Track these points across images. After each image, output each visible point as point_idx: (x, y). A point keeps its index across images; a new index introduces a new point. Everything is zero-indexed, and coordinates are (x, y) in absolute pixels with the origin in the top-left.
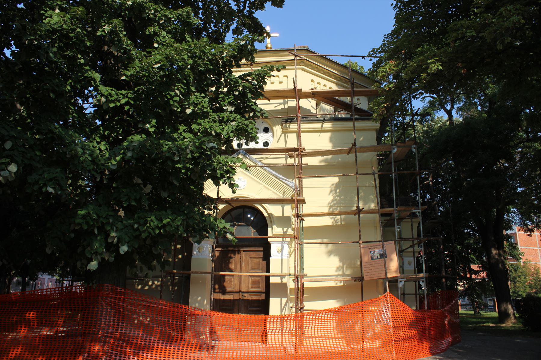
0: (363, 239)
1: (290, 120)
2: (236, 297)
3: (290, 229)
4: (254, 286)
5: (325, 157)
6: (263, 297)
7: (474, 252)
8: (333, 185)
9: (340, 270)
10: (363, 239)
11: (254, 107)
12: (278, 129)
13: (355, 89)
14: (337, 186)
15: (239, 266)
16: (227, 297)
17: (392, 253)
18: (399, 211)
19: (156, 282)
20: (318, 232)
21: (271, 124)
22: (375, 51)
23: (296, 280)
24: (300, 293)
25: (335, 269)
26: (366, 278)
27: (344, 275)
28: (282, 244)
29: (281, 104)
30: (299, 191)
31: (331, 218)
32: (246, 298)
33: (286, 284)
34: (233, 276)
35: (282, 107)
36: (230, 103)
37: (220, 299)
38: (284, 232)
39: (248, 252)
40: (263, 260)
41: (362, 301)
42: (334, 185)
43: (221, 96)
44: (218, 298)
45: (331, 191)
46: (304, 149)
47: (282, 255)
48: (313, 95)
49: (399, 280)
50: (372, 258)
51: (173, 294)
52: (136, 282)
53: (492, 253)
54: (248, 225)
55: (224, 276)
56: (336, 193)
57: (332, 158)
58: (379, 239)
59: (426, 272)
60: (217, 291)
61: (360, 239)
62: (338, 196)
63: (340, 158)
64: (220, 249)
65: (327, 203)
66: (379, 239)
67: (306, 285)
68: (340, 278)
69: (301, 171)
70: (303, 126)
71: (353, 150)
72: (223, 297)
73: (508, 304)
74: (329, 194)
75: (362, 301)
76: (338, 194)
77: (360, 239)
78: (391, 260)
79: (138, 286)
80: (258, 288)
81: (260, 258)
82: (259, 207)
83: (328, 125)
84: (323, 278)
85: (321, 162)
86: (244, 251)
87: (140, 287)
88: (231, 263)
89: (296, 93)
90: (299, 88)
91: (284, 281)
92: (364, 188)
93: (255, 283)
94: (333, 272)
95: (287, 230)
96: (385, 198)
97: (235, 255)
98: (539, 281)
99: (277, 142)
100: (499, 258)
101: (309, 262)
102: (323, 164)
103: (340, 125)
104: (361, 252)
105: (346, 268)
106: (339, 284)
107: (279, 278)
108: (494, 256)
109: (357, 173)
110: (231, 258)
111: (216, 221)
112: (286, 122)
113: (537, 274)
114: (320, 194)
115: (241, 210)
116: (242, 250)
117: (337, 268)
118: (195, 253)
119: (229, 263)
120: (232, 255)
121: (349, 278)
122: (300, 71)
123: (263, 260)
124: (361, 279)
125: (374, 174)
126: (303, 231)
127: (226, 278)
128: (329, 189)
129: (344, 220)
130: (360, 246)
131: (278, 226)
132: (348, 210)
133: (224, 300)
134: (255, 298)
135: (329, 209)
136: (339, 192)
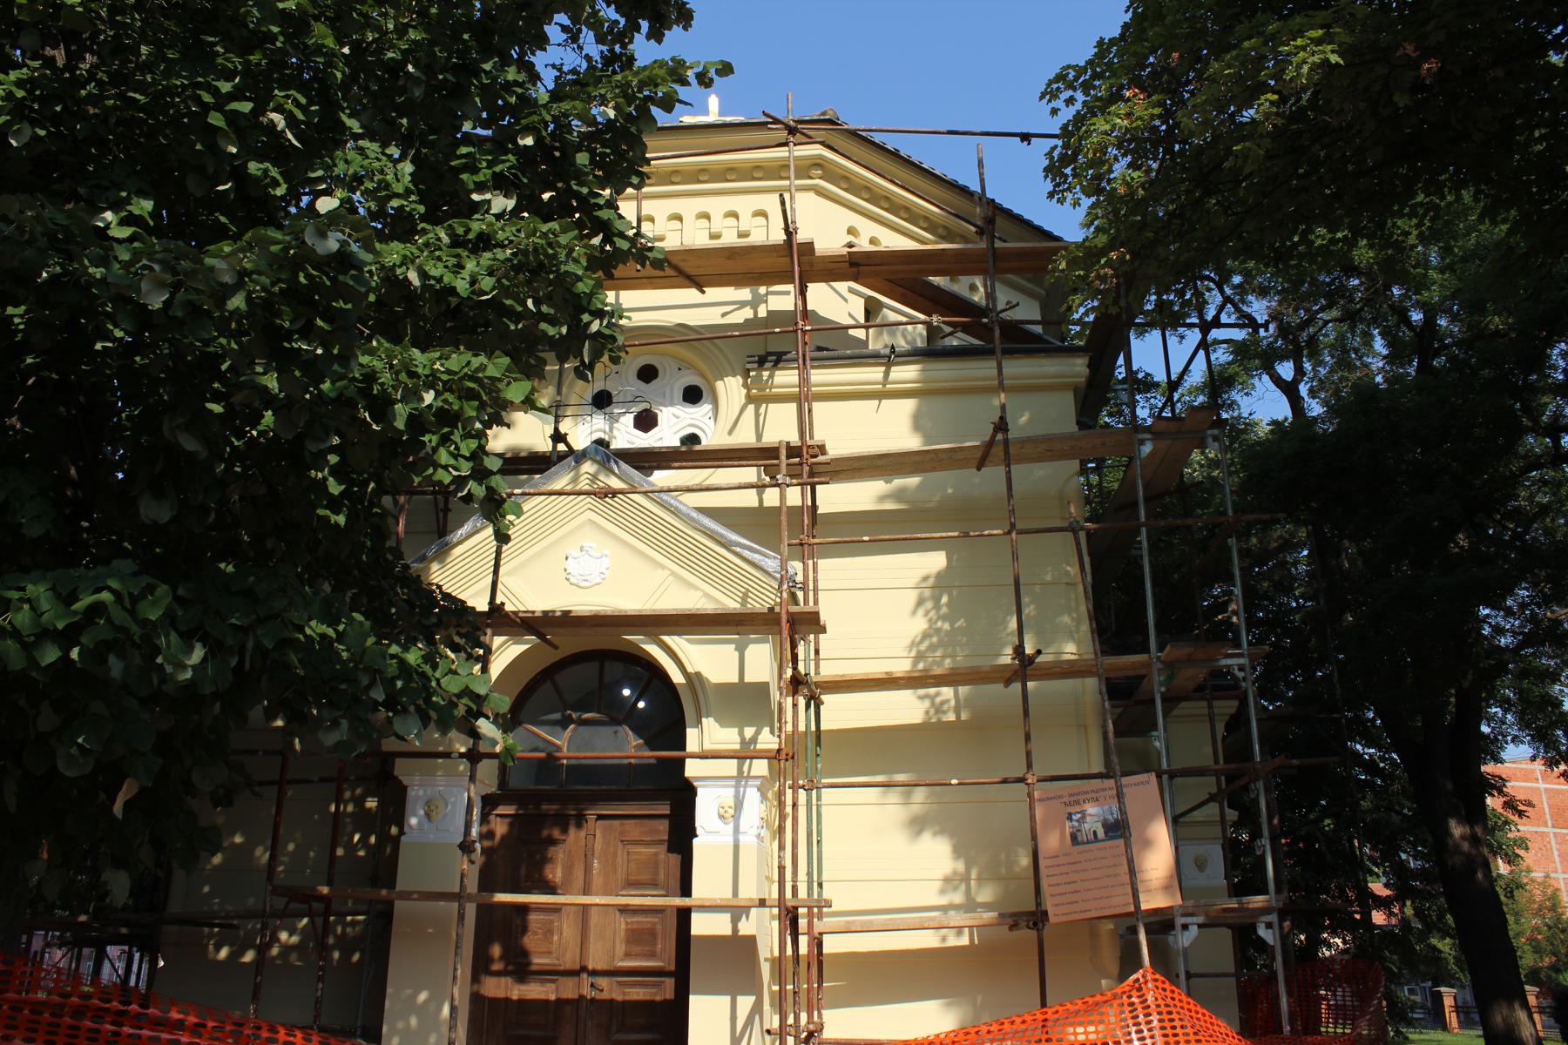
0: (1040, 769)
1: (778, 359)
2: (568, 989)
3: (766, 730)
4: (636, 949)
5: (898, 482)
6: (667, 989)
7: (1370, 836)
8: (925, 578)
9: (955, 889)
10: (1040, 769)
11: (605, 214)
12: (731, 389)
13: (998, 244)
14: (941, 583)
15: (579, 873)
16: (534, 991)
17: (1150, 818)
18: (1171, 667)
19: (284, 936)
20: (874, 752)
21: (710, 377)
22: (1072, 74)
23: (790, 918)
24: (810, 975)
25: (938, 884)
26: (1056, 912)
27: (970, 906)
28: (737, 787)
29: (743, 304)
30: (804, 588)
31: (921, 698)
32: (605, 996)
33: (751, 941)
34: (556, 909)
35: (747, 313)
36: (501, 184)
37: (507, 1000)
38: (743, 741)
39: (616, 823)
40: (670, 850)
41: (1044, 1004)
42: (931, 582)
43: (464, 150)
44: (501, 994)
45: (920, 602)
46: (822, 449)
47: (736, 831)
48: (854, 266)
49: (1180, 921)
50: (1074, 838)
51: (320, 979)
52: (211, 936)
53: (1450, 835)
54: (615, 721)
55: (524, 909)
56: (937, 607)
57: (920, 487)
58: (1097, 767)
59: (1278, 891)
60: (497, 966)
61: (1029, 766)
62: (944, 618)
63: (949, 483)
64: (510, 810)
65: (909, 641)
66: (1097, 767)
67: (831, 945)
68: (957, 918)
69: (811, 534)
70: (821, 377)
71: (998, 451)
72: (517, 991)
73: (1517, 1006)
74: (914, 612)
75: (1044, 1004)
76: (944, 610)
77: (1029, 766)
78: (1147, 843)
79: (218, 949)
80: (652, 955)
81: (660, 842)
82: (654, 650)
83: (906, 373)
84: (894, 918)
85: (882, 498)
86: (600, 817)
87: (224, 953)
88: (551, 860)
89: (795, 262)
90: (801, 237)
91: (745, 928)
92: (1037, 588)
93: (639, 939)
94: (931, 895)
95: (758, 733)
96: (1115, 624)
97: (565, 831)
98: (1563, 931)
99: (730, 433)
100: (1474, 852)
101: (838, 859)
102: (890, 506)
103: (947, 371)
104: (1032, 817)
105: (979, 879)
106: (953, 941)
107: (727, 917)
108: (1457, 846)
109: (1013, 526)
110: (553, 842)
111: (435, 667)
112: (761, 362)
113: (1553, 908)
114: (877, 610)
115: (591, 668)
116: (592, 813)
117: (947, 880)
118: (414, 821)
119: (546, 860)
120: (556, 833)
121: (989, 916)
122: (811, 195)
123: (670, 850)
124: (1037, 919)
125: (1073, 529)
126: (818, 743)
127: (533, 917)
128: (913, 596)
129: (968, 703)
130: (1029, 795)
131: (723, 722)
132: (984, 663)
133: (523, 1004)
134: (637, 994)
135: (915, 664)
136: (948, 605)
